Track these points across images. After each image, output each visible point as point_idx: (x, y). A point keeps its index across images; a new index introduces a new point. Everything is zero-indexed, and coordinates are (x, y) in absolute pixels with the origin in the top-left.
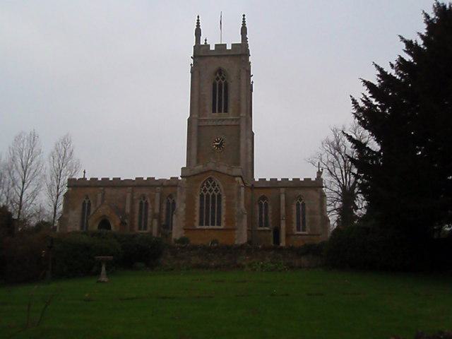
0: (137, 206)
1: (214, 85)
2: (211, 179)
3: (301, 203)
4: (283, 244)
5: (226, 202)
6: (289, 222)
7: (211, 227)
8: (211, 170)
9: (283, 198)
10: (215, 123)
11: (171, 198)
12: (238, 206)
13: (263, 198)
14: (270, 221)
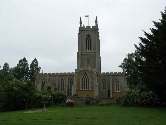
2: (85, 73)
4: (111, 96)
6: (113, 88)
7: (86, 90)
9: (111, 79)
13: (104, 79)
14: (106, 87)
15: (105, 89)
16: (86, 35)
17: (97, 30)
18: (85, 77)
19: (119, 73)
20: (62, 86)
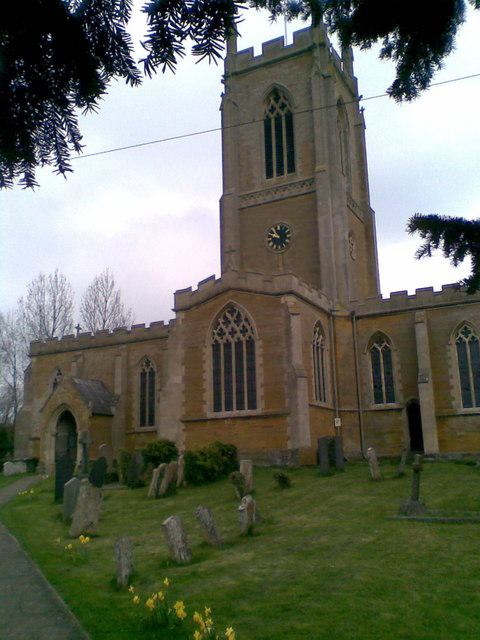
0: (137, 380)
1: (267, 122)
2: (232, 309)
3: (467, 340)
4: (431, 443)
5: (263, 355)
6: (441, 387)
7: (235, 412)
8: (230, 289)
9: (422, 332)
10: (269, 198)
11: (380, 342)
12: (289, 361)
13: (380, 338)
14: (398, 387)
15: (391, 399)
16: (260, 90)
17: (231, 80)
18: (233, 333)
19: (418, 290)
20: (143, 396)
